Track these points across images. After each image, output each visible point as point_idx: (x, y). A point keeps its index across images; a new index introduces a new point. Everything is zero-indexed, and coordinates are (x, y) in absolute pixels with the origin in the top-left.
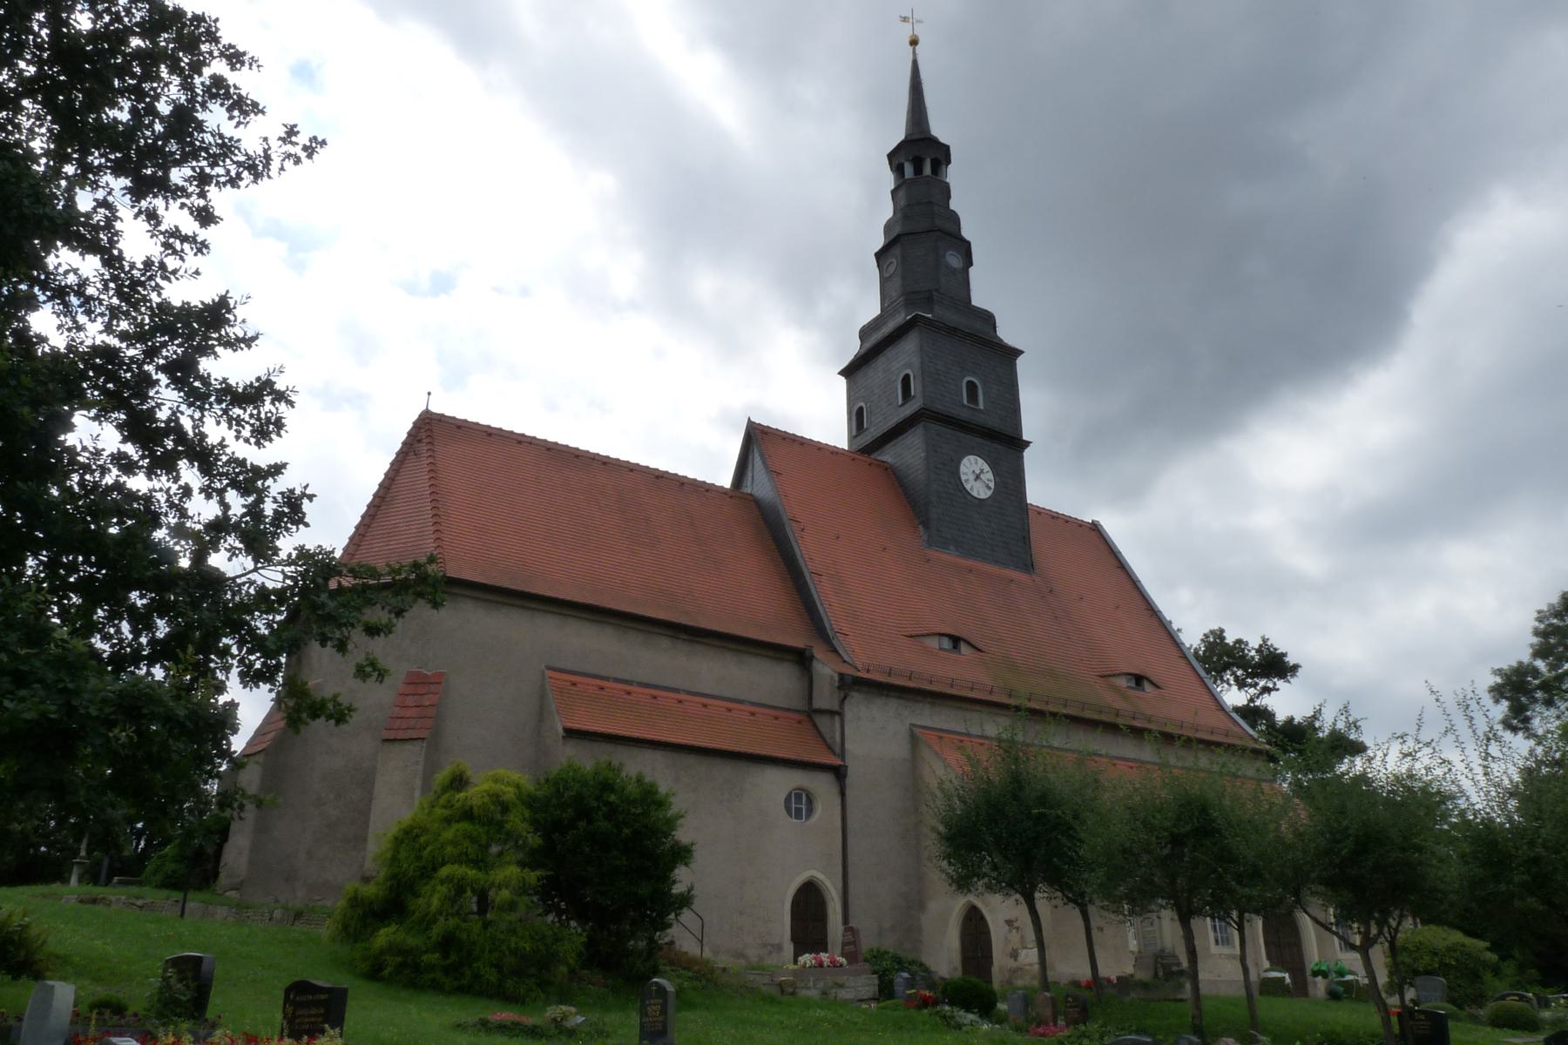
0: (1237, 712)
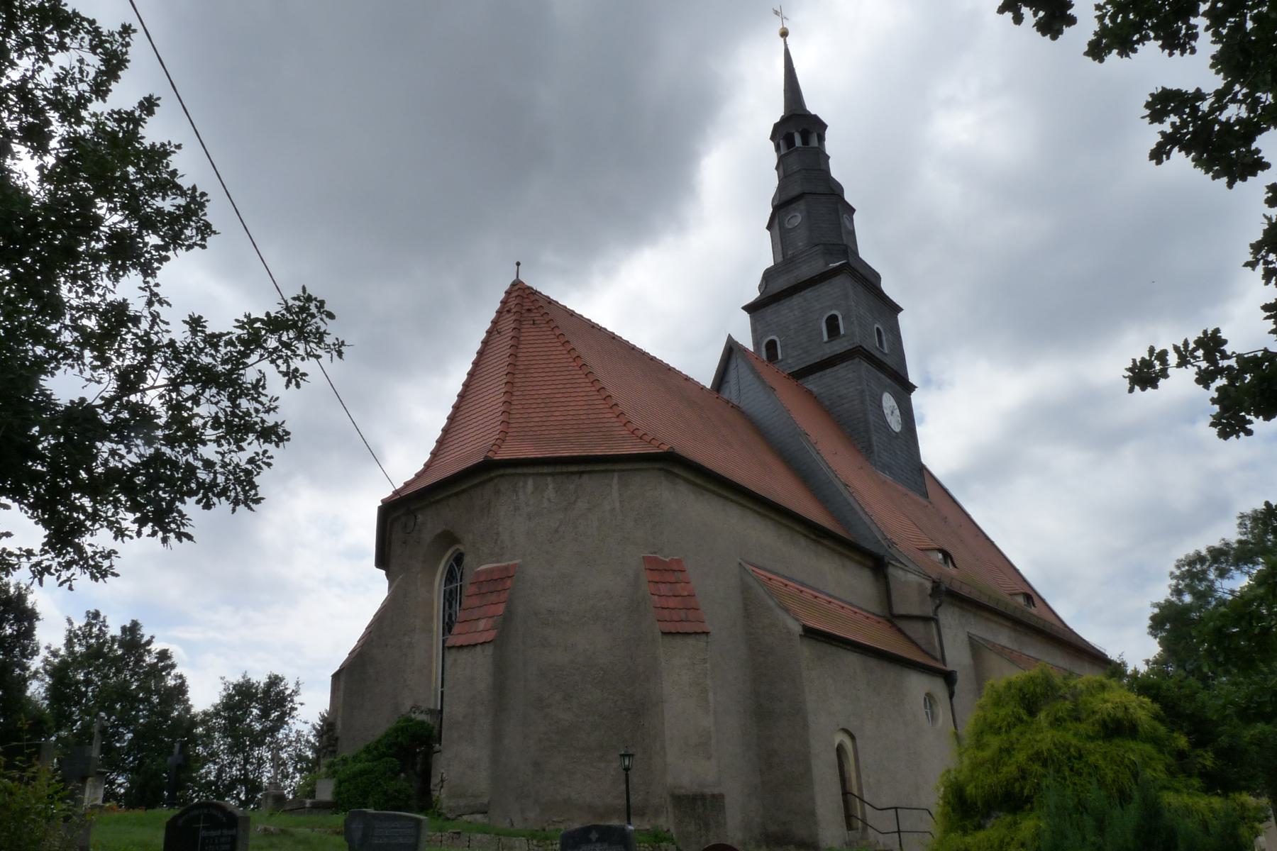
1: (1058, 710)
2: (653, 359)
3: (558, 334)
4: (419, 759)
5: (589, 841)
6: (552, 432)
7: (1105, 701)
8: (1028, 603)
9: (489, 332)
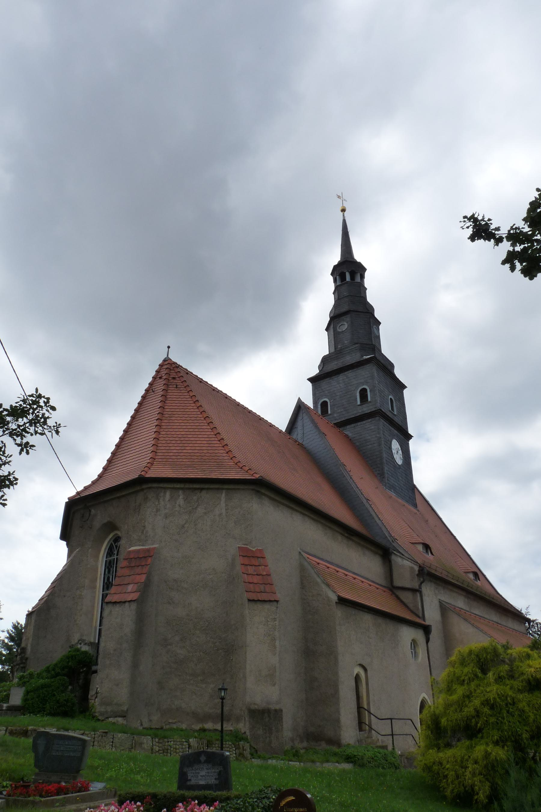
0: (70, 556)
1: (501, 671)
2: (250, 412)
3: (191, 395)
4: (82, 676)
5: (200, 762)
6: (184, 460)
7: (530, 666)
8: (476, 578)
9: (147, 391)
